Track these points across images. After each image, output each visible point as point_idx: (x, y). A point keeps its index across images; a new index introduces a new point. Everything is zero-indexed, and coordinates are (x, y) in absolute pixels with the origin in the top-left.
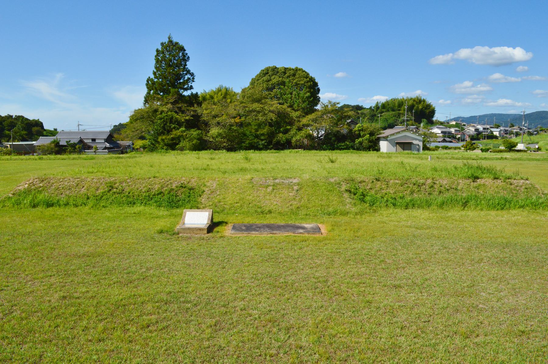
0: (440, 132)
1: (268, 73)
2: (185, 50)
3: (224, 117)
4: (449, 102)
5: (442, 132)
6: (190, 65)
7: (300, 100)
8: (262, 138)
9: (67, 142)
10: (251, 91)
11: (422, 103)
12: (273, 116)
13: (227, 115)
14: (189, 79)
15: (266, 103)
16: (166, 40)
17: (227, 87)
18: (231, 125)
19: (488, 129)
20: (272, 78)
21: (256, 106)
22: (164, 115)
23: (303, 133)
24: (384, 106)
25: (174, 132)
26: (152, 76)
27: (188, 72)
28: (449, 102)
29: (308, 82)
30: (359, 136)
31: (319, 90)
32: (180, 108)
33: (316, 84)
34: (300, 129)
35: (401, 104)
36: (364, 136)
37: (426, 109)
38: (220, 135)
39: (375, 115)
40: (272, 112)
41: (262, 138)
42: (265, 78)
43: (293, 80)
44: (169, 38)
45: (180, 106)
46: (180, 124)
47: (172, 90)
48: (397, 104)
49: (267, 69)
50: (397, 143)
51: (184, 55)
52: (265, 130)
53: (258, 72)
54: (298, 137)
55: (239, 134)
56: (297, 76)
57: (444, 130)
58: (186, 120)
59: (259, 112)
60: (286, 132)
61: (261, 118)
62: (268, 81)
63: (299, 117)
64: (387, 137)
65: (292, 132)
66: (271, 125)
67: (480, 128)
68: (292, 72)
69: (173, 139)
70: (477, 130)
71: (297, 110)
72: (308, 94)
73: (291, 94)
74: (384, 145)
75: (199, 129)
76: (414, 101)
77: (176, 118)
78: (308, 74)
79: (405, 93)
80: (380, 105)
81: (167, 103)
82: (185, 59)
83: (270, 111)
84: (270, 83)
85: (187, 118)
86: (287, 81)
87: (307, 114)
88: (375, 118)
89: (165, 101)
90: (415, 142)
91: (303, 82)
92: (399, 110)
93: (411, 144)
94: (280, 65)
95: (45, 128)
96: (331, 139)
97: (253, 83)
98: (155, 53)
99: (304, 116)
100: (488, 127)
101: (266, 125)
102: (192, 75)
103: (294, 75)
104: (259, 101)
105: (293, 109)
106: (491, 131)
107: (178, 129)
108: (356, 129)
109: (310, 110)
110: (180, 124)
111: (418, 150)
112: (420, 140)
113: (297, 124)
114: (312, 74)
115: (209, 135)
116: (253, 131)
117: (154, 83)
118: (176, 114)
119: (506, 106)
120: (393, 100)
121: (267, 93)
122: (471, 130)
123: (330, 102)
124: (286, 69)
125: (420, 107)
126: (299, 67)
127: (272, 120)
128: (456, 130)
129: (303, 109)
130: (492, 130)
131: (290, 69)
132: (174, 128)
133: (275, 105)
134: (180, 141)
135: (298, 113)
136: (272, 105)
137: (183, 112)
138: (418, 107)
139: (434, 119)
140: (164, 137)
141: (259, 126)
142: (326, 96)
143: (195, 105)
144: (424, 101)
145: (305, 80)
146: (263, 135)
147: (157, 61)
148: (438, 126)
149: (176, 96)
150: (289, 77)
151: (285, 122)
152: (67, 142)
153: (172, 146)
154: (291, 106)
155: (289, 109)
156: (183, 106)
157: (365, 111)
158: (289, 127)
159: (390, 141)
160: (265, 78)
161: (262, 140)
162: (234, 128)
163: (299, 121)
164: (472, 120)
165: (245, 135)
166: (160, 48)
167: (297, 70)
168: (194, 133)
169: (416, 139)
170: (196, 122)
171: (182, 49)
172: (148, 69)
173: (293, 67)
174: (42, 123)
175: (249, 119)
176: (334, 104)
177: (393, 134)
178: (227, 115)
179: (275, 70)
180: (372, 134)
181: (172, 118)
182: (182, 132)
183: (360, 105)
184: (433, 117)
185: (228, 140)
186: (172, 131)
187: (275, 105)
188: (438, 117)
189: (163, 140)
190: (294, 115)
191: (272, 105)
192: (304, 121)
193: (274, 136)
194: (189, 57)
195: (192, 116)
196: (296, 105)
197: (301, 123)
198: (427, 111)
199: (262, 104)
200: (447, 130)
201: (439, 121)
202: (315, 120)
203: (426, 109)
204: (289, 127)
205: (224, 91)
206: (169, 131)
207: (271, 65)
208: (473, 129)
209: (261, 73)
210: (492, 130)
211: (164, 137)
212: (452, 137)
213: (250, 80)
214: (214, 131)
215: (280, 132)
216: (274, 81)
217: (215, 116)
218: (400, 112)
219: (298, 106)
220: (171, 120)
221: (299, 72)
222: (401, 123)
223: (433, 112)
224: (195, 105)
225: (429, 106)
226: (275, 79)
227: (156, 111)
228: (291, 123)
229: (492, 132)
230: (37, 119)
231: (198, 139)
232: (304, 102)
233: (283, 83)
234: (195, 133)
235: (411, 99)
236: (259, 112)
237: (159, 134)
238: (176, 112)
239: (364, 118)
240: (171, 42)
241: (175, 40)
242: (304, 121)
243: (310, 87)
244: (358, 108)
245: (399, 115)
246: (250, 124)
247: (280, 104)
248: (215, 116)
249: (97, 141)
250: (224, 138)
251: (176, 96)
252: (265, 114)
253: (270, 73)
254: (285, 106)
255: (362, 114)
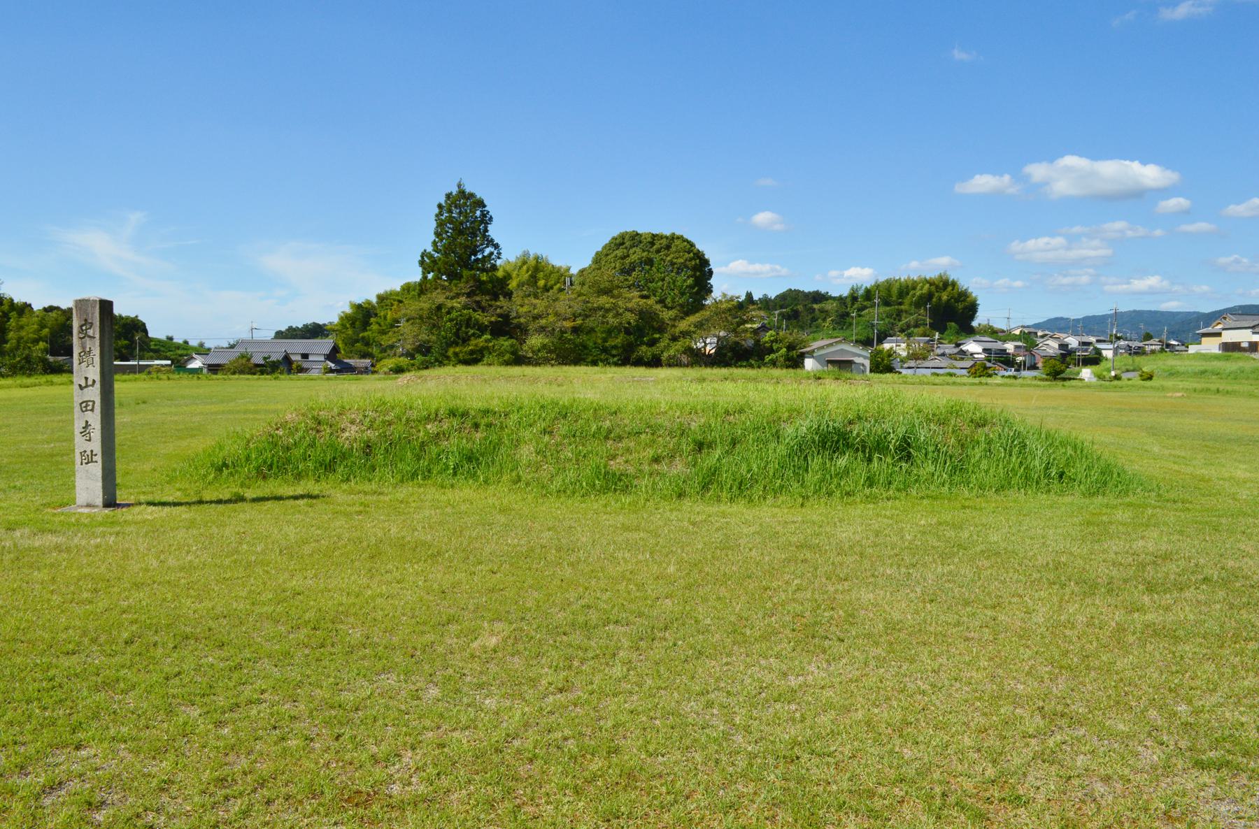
0: (980, 350)
1: (623, 244)
2: (485, 206)
3: (551, 318)
4: (1018, 284)
5: (985, 350)
6: (494, 231)
7: (676, 291)
8: (614, 352)
9: (265, 358)
10: (594, 274)
11: (950, 288)
12: (631, 318)
13: (557, 314)
14: (492, 253)
15: (619, 296)
16: (455, 191)
17: (539, 254)
18: (562, 332)
19: (1089, 344)
20: (631, 251)
21: (604, 300)
22: (454, 314)
23: (679, 345)
24: (869, 294)
25: (473, 342)
26: (430, 249)
27: (491, 242)
28: (1018, 284)
29: (691, 260)
30: (771, 351)
31: (711, 272)
32: (478, 303)
33: (705, 262)
34: (674, 339)
35: (905, 289)
36: (778, 350)
37: (957, 300)
38: (544, 346)
39: (848, 314)
40: (631, 310)
41: (614, 352)
42: (619, 253)
43: (667, 255)
44: (459, 186)
45: (478, 298)
46: (482, 329)
47: (466, 273)
48: (895, 291)
49: (623, 236)
50: (829, 362)
51: (484, 215)
52: (619, 340)
53: (607, 240)
54: (672, 352)
55: (576, 346)
56: (673, 249)
57: (988, 346)
58: (491, 322)
59: (608, 311)
60: (653, 343)
61: (612, 320)
62: (623, 258)
63: (674, 320)
64: (813, 351)
65: (662, 344)
66: (628, 332)
67: (1073, 342)
68: (664, 242)
69: (472, 353)
70: (1063, 346)
71: (672, 308)
72: (690, 281)
73: (663, 280)
74: (809, 363)
75: (512, 337)
76: (931, 283)
77: (477, 320)
78: (692, 245)
79: (917, 265)
80: (861, 292)
81: (458, 295)
82: (486, 219)
83: (627, 310)
84: (627, 261)
85: (493, 319)
86: (656, 258)
87: (687, 314)
88: (848, 320)
89: (455, 290)
90: (857, 360)
91: (682, 260)
92: (900, 304)
93: (850, 363)
94: (646, 227)
95: (150, 335)
96: (725, 355)
97: (598, 259)
98: (437, 211)
99: (682, 318)
100: (1093, 339)
101: (620, 331)
102: (496, 246)
103: (668, 247)
104: (607, 292)
105: (665, 306)
106: (1096, 349)
107: (480, 337)
108: (767, 339)
109: (697, 306)
110: (482, 329)
111: (863, 372)
112: (865, 358)
113: (671, 331)
114: (700, 246)
115: (525, 348)
116: (599, 341)
117: (434, 262)
118: (470, 298)
119: (1152, 292)
120: (889, 285)
121: (622, 278)
122: (1052, 347)
123: (725, 295)
124: (654, 236)
125: (945, 298)
126: (678, 233)
127: (629, 323)
128: (1016, 347)
129: (681, 306)
130: (1099, 346)
131: (662, 237)
132: (473, 334)
133: (633, 299)
134: (483, 356)
135: (672, 313)
136: (630, 300)
137: (484, 310)
138: (940, 298)
139: (975, 324)
140: (457, 350)
141: (609, 332)
142: (728, 283)
143: (501, 298)
144: (954, 284)
145: (687, 255)
146: (615, 347)
147: (441, 224)
148: (978, 338)
149: (472, 283)
150: (658, 251)
151: (653, 327)
152: (265, 358)
153: (473, 359)
154: (662, 301)
155: (658, 307)
156: (484, 299)
157: (829, 306)
158: (657, 336)
159: (818, 359)
160: (619, 253)
161: (614, 356)
162: (568, 336)
163: (674, 326)
164: (1058, 325)
165: (585, 347)
166: (442, 200)
167: (673, 238)
168: (505, 343)
169: (859, 356)
170: (505, 327)
171: (481, 204)
172: (425, 238)
173: (668, 233)
174: (144, 324)
175: (590, 323)
176: (732, 299)
177: (822, 348)
178: (557, 314)
179: (635, 238)
180: (791, 347)
181: (470, 318)
182: (487, 341)
183: (823, 291)
184: (972, 317)
185: (558, 355)
186: (469, 339)
187: (633, 299)
188: (979, 321)
189: (456, 354)
190: (667, 315)
191: (630, 300)
192: (683, 325)
193: (636, 345)
194: (491, 218)
195: (500, 316)
196: (669, 300)
197: (677, 330)
198: (960, 306)
199: (612, 297)
200: (999, 345)
201: (991, 327)
202: (699, 325)
203: (957, 300)
204: (657, 336)
205: (532, 262)
206: (465, 341)
207: (629, 229)
208: (1055, 344)
209: (611, 243)
210: (1099, 346)
211: (457, 350)
212: (1006, 361)
213: (593, 255)
214: (535, 341)
215: (642, 343)
216: (634, 258)
217: (536, 318)
218: (902, 307)
219: (673, 301)
220: (468, 322)
221: (677, 242)
222: (902, 331)
223: (972, 309)
224: (501, 298)
225: (964, 295)
226: (636, 255)
227: (439, 308)
228: (661, 329)
229: (1098, 352)
230: (133, 316)
231: (512, 353)
232: (683, 294)
233: (650, 262)
234: (506, 343)
235: (927, 281)
236: (608, 311)
237: (450, 344)
238: (474, 310)
239: (824, 320)
240: (462, 193)
241: (468, 189)
242: (683, 325)
243: (694, 269)
244: (818, 297)
245: (899, 314)
246: (592, 330)
247: (643, 297)
248: (536, 318)
249: (311, 358)
250: (550, 352)
251: (472, 283)
252: (618, 315)
253: (628, 244)
254: (651, 301)
255: (822, 311)
